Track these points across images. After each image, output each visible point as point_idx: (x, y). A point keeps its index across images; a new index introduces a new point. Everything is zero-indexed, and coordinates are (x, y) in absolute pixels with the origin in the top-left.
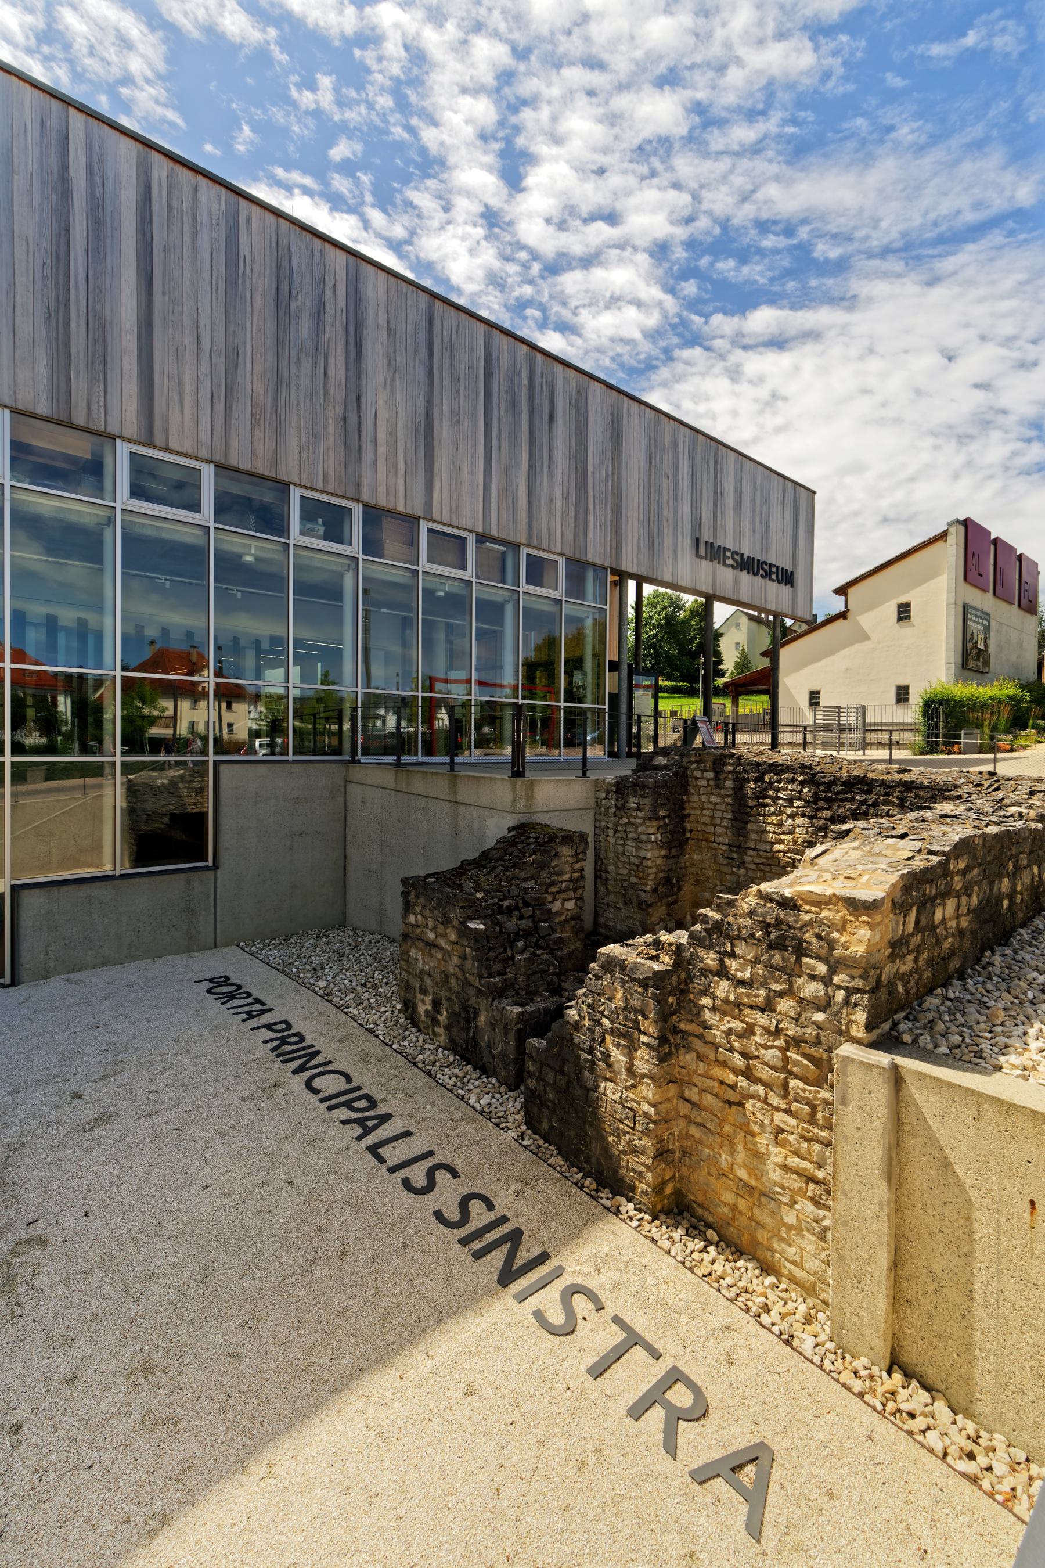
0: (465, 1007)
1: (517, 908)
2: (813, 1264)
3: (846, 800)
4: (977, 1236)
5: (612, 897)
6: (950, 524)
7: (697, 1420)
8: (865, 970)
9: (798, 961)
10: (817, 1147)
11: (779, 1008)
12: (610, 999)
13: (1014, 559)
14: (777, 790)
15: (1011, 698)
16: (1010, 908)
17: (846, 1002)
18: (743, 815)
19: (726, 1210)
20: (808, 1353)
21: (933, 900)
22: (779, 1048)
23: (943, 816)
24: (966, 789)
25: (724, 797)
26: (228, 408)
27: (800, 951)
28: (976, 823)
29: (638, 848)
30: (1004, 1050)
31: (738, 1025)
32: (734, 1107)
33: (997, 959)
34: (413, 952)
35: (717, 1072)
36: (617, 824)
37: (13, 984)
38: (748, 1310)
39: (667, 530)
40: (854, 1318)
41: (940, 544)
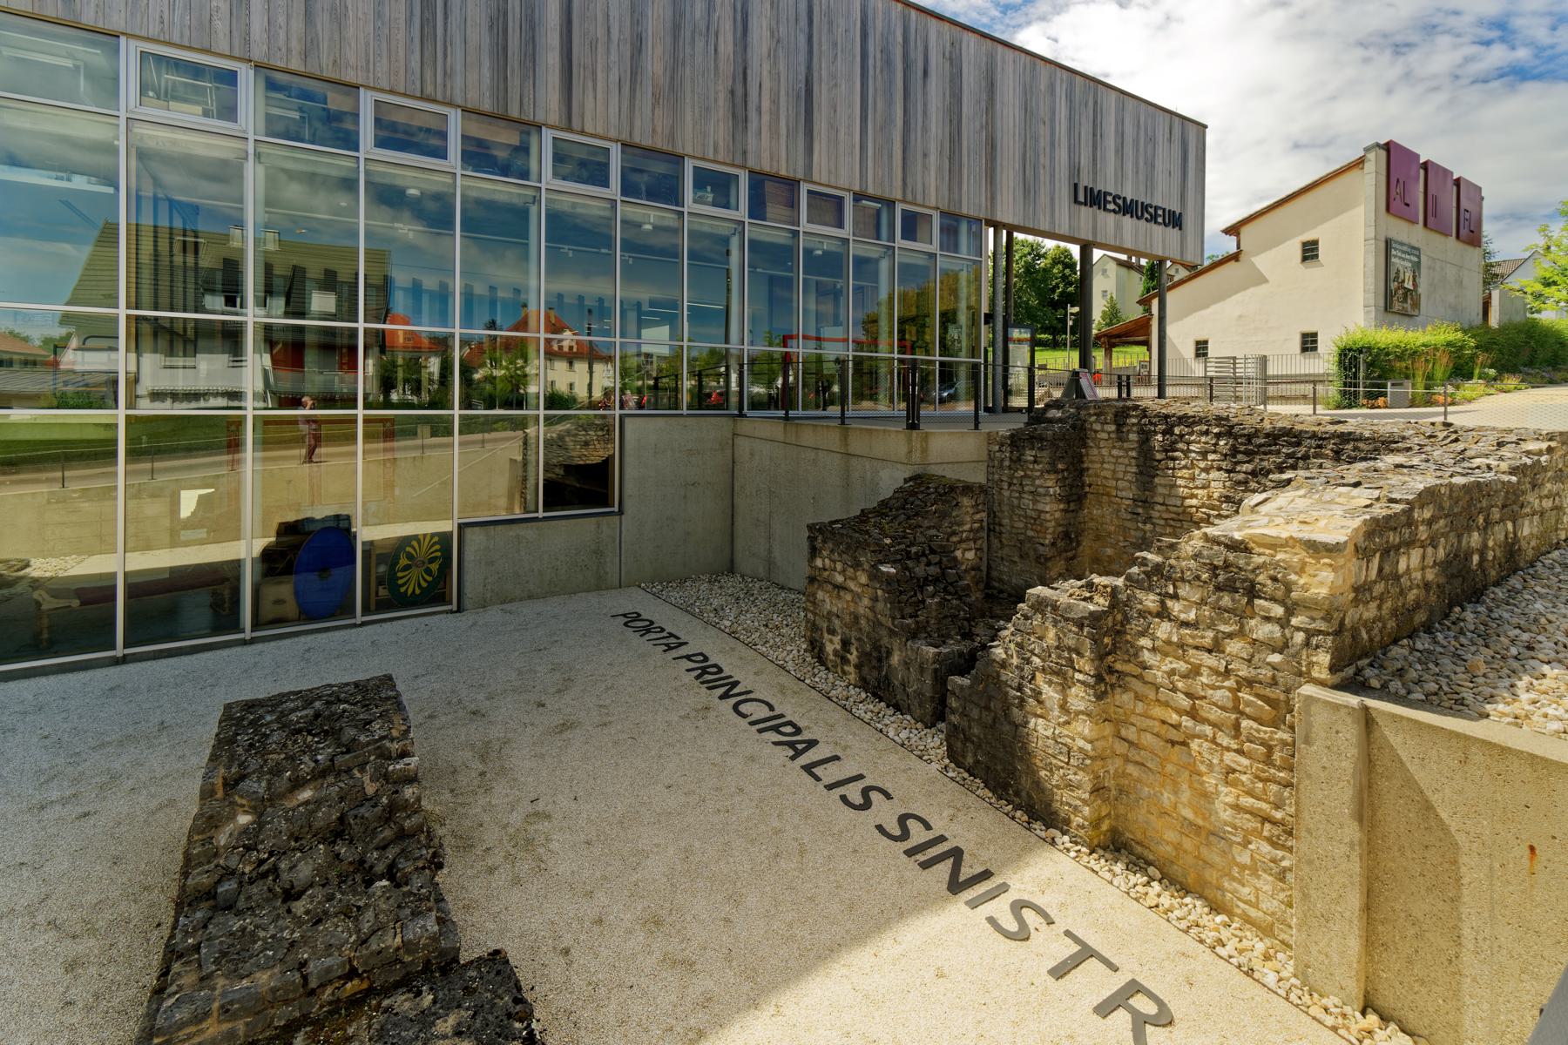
0: (877, 647)
1: (924, 554)
2: (1270, 905)
3: (1270, 452)
4: (1465, 881)
5: (1006, 551)
6: (1367, 150)
7: (1164, 1026)
8: (1328, 612)
9: (1250, 603)
10: (1274, 788)
11: (1228, 649)
12: (1040, 638)
13: (1450, 183)
14: (1188, 443)
15: (1449, 344)
16: (1480, 563)
17: (1307, 644)
18: (1148, 468)
19: (1169, 848)
20: (1273, 985)
21: (1397, 548)
22: (1230, 689)
23: (1397, 466)
24: (1416, 440)
25: (1127, 450)
26: (633, 91)
27: (1252, 592)
28: (1439, 473)
29: (1035, 502)
30: (1491, 699)
31: (1182, 666)
32: (1177, 747)
33: (1469, 615)
34: (820, 595)
35: (1158, 712)
36: (1012, 477)
37: (459, 611)
38: (1202, 941)
39: (1044, 176)
40: (1322, 957)
41: (1355, 173)
